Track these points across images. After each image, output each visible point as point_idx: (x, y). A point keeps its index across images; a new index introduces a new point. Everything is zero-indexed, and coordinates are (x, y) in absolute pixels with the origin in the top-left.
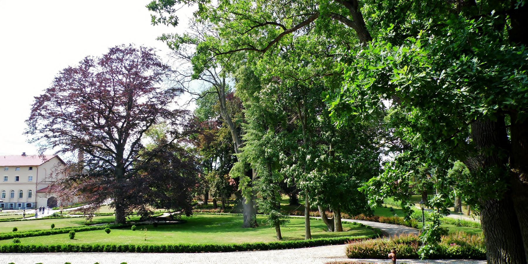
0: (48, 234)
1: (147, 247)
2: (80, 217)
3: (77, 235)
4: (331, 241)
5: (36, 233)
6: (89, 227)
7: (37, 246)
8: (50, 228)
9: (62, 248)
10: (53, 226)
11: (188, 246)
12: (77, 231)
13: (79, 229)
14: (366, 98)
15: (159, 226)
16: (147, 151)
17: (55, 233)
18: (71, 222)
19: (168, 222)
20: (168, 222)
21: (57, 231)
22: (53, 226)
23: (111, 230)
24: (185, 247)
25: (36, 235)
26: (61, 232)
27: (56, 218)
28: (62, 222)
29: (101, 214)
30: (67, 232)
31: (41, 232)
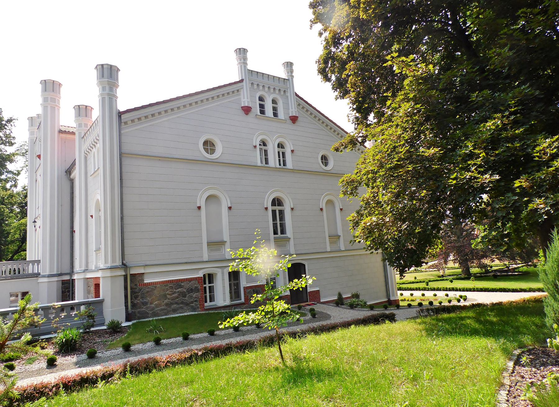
0: (413, 283)
1: (464, 288)
2: (435, 271)
3: (430, 283)
4: (484, 289)
5: (407, 282)
6: (439, 279)
7: (409, 288)
8: (414, 279)
9: (421, 289)
10: (415, 278)
11: (488, 289)
12: (430, 281)
13: (432, 280)
14: (189, 312)
15: (498, 277)
16: (377, 28)
17: (417, 282)
18: (428, 275)
19: (511, 273)
20: (511, 273)
21: (418, 281)
22: (415, 278)
23: (453, 280)
24: (486, 289)
25: (407, 283)
26: (421, 282)
27: (417, 272)
28: (422, 275)
29: (452, 268)
30: (424, 282)
31: (409, 282)
